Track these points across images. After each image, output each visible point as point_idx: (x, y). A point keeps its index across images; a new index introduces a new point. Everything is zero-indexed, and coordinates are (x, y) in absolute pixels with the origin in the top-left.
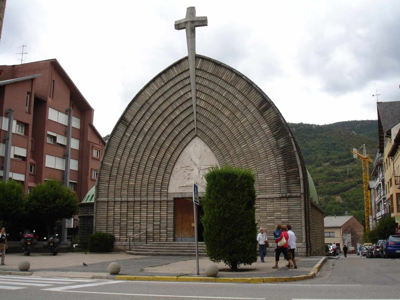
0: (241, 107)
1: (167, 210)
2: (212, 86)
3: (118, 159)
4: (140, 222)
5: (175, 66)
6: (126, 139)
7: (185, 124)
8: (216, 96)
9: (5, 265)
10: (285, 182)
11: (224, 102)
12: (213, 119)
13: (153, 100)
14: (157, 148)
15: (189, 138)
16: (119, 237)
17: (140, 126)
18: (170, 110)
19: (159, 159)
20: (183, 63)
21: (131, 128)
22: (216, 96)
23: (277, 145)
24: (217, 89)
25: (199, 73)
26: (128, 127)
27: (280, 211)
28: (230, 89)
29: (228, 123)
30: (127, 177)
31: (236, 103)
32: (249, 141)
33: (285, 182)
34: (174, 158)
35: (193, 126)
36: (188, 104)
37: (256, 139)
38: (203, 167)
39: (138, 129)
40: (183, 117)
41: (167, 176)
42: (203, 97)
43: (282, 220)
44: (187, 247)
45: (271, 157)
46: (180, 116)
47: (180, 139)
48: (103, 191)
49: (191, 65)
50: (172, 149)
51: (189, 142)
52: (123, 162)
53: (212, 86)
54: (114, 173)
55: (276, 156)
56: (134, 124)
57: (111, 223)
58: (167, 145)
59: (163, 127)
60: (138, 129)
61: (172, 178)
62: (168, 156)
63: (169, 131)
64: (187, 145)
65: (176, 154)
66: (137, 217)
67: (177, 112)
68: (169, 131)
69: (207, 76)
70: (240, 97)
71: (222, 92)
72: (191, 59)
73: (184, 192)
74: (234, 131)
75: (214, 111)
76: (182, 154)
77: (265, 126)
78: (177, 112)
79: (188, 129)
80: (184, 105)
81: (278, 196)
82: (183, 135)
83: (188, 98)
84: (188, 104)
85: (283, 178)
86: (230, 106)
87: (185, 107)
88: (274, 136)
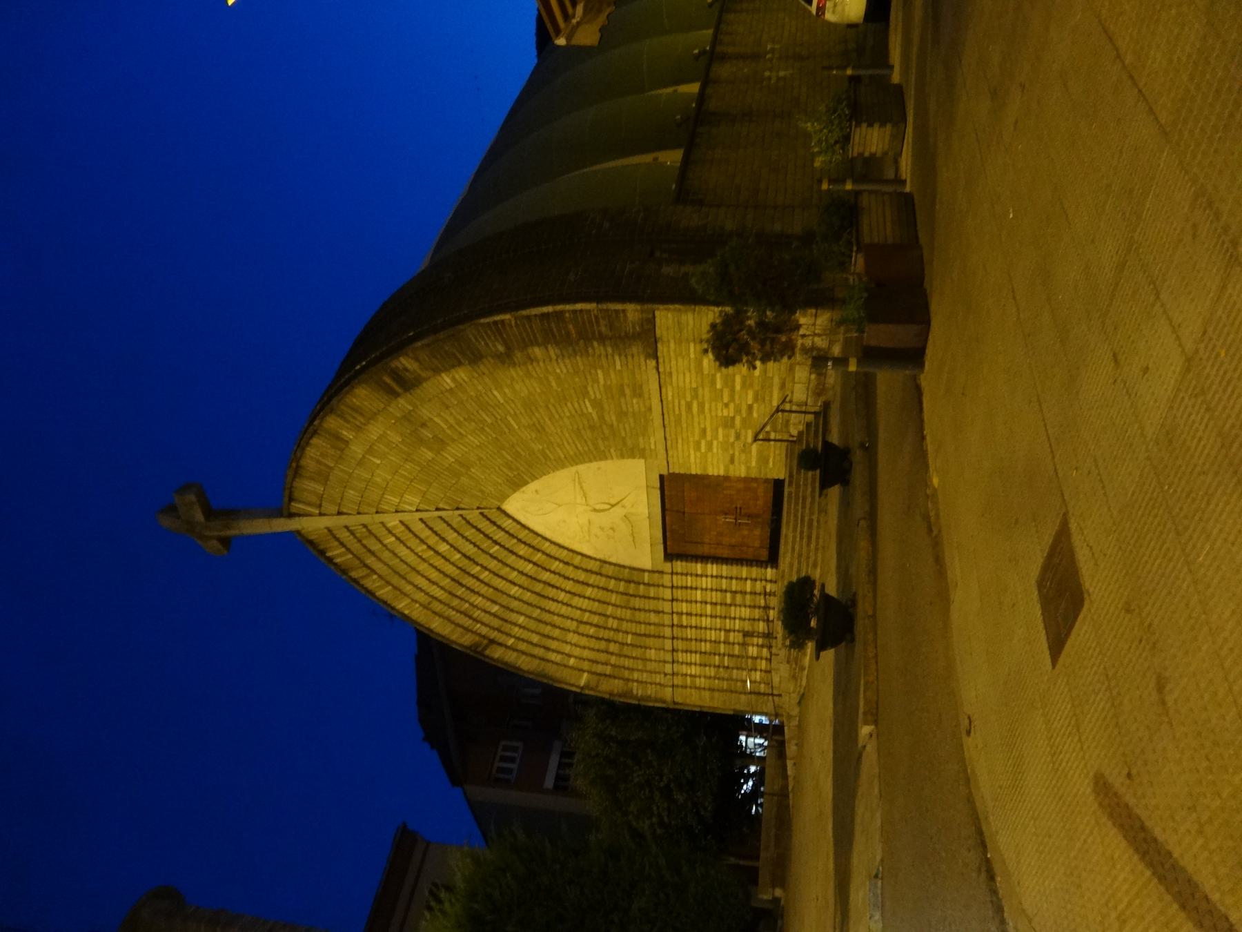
1: (697, 575)
3: (572, 661)
4: (725, 630)
5: (325, 553)
6: (523, 646)
7: (470, 533)
9: (818, 657)
14: (539, 587)
15: (507, 524)
16: (758, 673)
19: (569, 585)
21: (494, 635)
30: (613, 647)
34: (563, 554)
39: (496, 623)
40: (451, 536)
41: (609, 570)
44: (797, 504)
46: (451, 542)
47: (511, 543)
50: (538, 557)
51: (518, 522)
52: (577, 652)
54: (608, 670)
56: (484, 630)
57: (725, 685)
58: (529, 568)
59: (485, 575)
60: (496, 623)
61: (613, 560)
62: (556, 565)
63: (493, 564)
64: (524, 526)
65: (553, 550)
66: (712, 635)
67: (443, 548)
68: (493, 564)
76: (550, 538)
78: (443, 548)
79: (484, 525)
80: (423, 536)
83: (403, 528)
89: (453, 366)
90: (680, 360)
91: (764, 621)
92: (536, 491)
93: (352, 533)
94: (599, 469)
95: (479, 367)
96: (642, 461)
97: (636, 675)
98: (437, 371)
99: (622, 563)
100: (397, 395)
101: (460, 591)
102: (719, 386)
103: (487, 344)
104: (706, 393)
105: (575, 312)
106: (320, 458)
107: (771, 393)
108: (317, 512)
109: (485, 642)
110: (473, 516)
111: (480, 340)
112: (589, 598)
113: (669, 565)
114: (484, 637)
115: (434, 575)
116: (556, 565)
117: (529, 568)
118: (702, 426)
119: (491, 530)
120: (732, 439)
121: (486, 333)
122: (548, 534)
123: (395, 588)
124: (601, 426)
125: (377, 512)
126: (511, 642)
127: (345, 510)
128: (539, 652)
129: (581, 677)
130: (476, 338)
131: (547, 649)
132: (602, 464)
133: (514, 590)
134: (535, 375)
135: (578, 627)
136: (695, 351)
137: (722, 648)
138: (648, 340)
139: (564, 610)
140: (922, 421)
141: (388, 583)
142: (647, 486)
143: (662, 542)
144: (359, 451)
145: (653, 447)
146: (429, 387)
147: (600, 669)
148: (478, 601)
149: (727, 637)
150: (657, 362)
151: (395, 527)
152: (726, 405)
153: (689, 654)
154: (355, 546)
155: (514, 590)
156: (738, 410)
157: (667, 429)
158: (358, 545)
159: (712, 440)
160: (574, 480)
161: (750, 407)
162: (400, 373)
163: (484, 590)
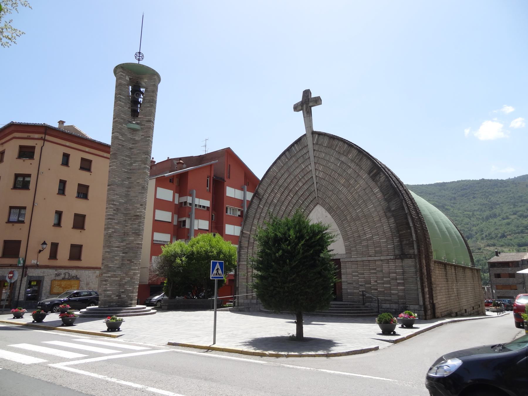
6: (259, 211)
7: (307, 193)
13: (279, 175)
17: (271, 198)
21: (264, 201)
26: (261, 200)
27: (395, 273)
40: (306, 187)
45: (384, 220)
49: (309, 141)
55: (388, 218)
56: (265, 197)
67: (300, 184)
72: (309, 136)
78: (300, 184)
79: (311, 198)
82: (306, 203)
85: (396, 240)
89: (383, 193)
90: (394, 267)
91: (252, 298)
92: (327, 216)
93: (306, 154)
95: (383, 201)
97: (250, 251)
98: (381, 188)
100: (369, 174)
101: (282, 189)
102: (384, 279)
103: (394, 204)
104: (380, 275)
105: (411, 232)
106: (338, 146)
107: (383, 297)
108: (315, 143)
109: (261, 197)
110: (315, 195)
111: (395, 202)
114: (263, 197)
115: (289, 180)
118: (365, 274)
119: (309, 200)
120: (360, 283)
121: (398, 204)
123: (282, 167)
124: (360, 239)
125: (315, 163)
127: (315, 152)
128: (258, 216)
129: (248, 231)
130: (395, 201)
131: (259, 219)
133: (283, 208)
134: (134, 182)
136: (399, 272)
138: (402, 256)
140: (390, 342)
141: (284, 165)
144: (343, 159)
145: (352, 257)
146: (372, 184)
148: (278, 195)
150: (392, 259)
151: (309, 168)
152: (376, 281)
154: (300, 154)
155: (283, 208)
156: (374, 285)
157: (362, 262)
158: (301, 155)
159: (358, 277)
161: (377, 290)
162: (378, 175)
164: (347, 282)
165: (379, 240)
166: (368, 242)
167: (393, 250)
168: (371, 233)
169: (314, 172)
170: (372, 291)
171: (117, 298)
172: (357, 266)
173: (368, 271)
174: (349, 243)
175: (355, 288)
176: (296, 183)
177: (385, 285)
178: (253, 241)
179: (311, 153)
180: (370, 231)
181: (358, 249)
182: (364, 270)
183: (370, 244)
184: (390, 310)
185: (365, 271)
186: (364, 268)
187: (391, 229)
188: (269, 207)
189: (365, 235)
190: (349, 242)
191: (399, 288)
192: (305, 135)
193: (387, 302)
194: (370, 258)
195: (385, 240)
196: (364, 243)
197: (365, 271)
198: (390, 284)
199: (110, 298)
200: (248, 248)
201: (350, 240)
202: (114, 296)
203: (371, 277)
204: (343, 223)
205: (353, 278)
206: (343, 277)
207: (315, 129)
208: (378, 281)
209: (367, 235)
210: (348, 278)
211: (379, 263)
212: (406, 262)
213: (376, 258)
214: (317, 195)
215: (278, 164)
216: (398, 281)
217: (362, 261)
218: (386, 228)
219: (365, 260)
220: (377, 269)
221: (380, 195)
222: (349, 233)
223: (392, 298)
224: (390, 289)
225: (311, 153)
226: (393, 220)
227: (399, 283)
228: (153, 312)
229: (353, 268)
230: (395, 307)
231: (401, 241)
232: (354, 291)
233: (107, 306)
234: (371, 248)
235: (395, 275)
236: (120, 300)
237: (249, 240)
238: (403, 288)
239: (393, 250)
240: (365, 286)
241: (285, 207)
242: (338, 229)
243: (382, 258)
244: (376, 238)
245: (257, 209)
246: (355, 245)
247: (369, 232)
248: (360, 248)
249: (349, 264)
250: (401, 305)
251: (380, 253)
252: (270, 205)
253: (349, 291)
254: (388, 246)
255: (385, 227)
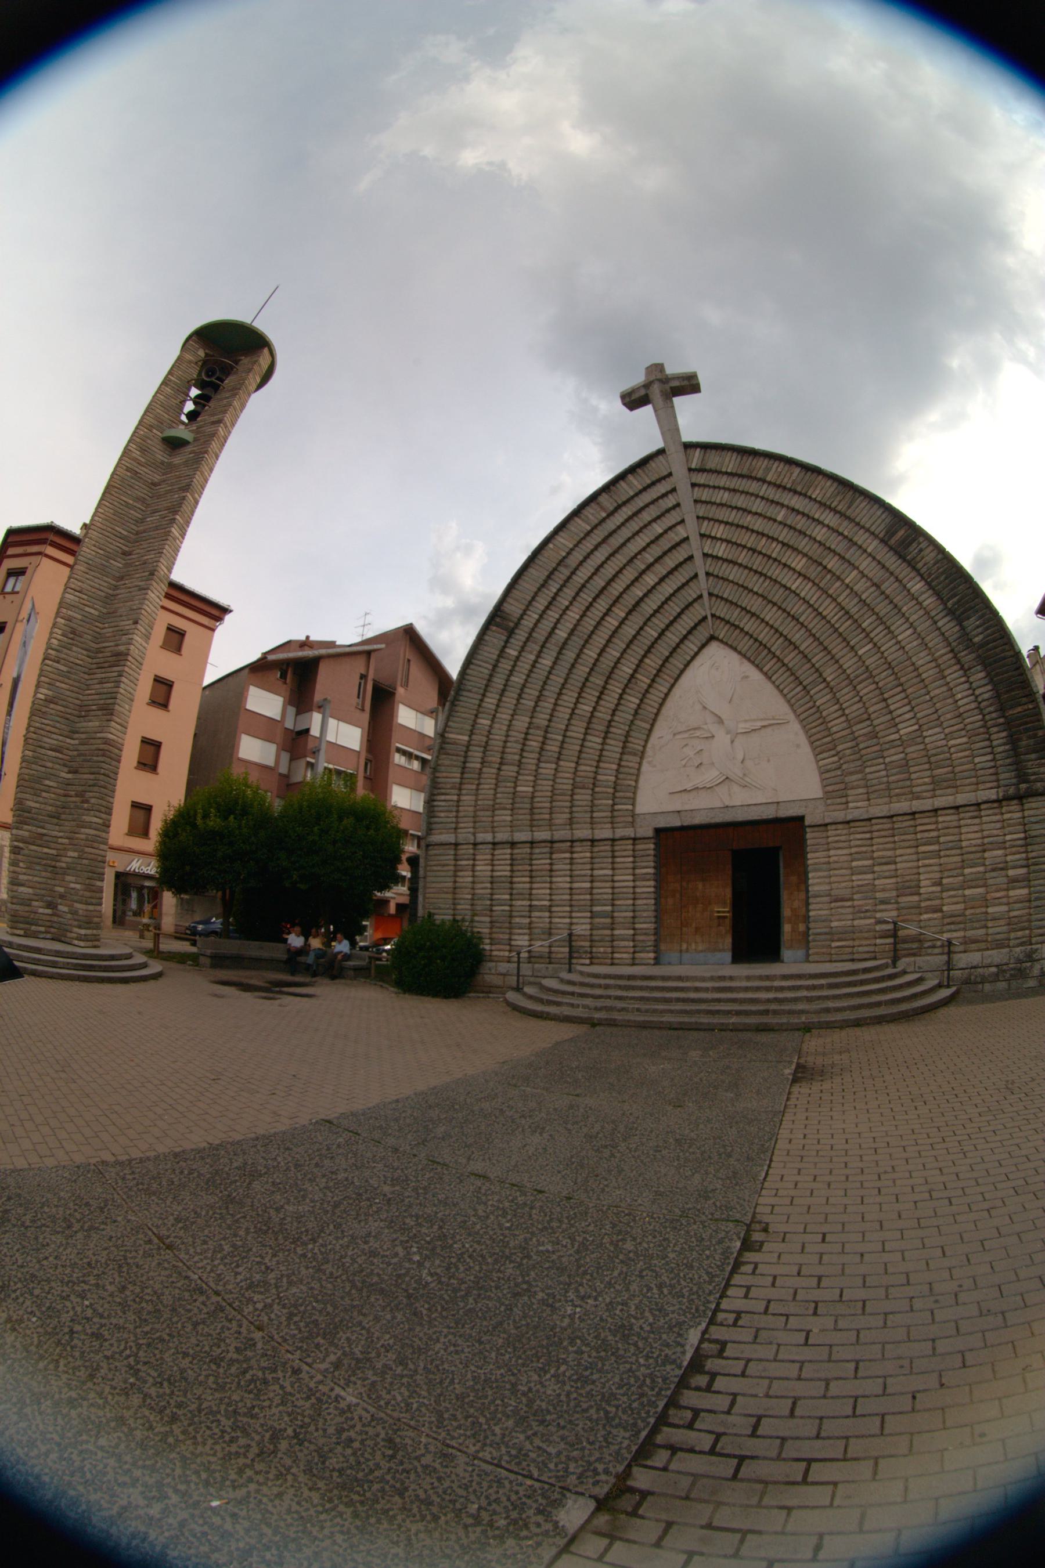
0: (834, 542)
2: (740, 501)
3: (484, 722)
6: (505, 665)
8: (758, 524)
10: (1007, 747)
11: (784, 535)
12: (757, 584)
15: (691, 646)
18: (629, 575)
20: (652, 464)
21: (521, 635)
22: (758, 524)
23: (965, 637)
24: (758, 506)
25: (701, 479)
26: (511, 633)
27: (1002, 845)
28: (796, 502)
29: (806, 590)
30: (509, 770)
31: (820, 533)
32: (878, 634)
33: (1007, 747)
34: (650, 709)
35: (698, 611)
36: (680, 555)
37: (897, 625)
38: (742, 725)
42: (719, 531)
43: (1011, 873)
45: (954, 675)
48: (442, 815)
49: (677, 463)
50: (643, 680)
51: (693, 658)
52: (500, 730)
53: (740, 501)
54: (474, 764)
55: (965, 670)
56: (528, 623)
59: (612, 622)
60: (540, 635)
62: (632, 701)
63: (629, 631)
65: (655, 696)
68: (629, 631)
69: (723, 481)
70: (829, 518)
71: (771, 511)
73: (687, 807)
74: (828, 608)
75: (757, 563)
77: (917, 586)
78: (650, 579)
81: (992, 795)
84: (680, 555)
85: (999, 737)
86: (803, 544)
87: (670, 562)
88: (951, 612)
94: (798, 746)
96: (820, 794)
97: (467, 799)
99: (33, 978)
112: (783, 505)
113: (650, 833)
116: (632, 701)
117: (627, 669)
120: (878, 895)
122: (677, 691)
126: (513, 652)
132: (806, 749)
135: (538, 728)
137: (521, 904)
139: (564, 713)
142: (778, 803)
143: (685, 824)
147: (476, 754)
149: (541, 909)
153: (548, 717)
160: (774, 719)
163: (589, 623)
164: (829, 895)
165: (944, 742)
166: (908, 750)
167: (991, 771)
168: (914, 721)
169: (695, 540)
170: (925, 916)
171: (49, 911)
172: (868, 836)
173: (909, 851)
174: (835, 759)
175: (859, 912)
176: (749, 545)
177: (967, 892)
178: (478, 766)
179: (685, 495)
180: (911, 715)
181: (869, 776)
182: (895, 849)
183: (914, 755)
184: (979, 970)
185: (898, 852)
186: (896, 838)
187: (980, 703)
188: (540, 652)
189: (893, 730)
190: (834, 756)
191: (1011, 893)
192: (661, 452)
193: (974, 946)
194: (917, 805)
195: (965, 740)
196: (894, 756)
197: (898, 852)
198: (985, 886)
199: (27, 908)
200: (460, 789)
201: (839, 748)
202: (41, 904)
203: (921, 870)
204: (812, 692)
205: (854, 878)
206: (813, 878)
207: (686, 437)
208: (945, 881)
209: (900, 726)
210: (833, 879)
211: (948, 818)
212: (1034, 805)
213: (939, 802)
214: (711, 609)
215: (571, 527)
216: (1011, 873)
217: (888, 817)
218: (965, 702)
219: (901, 812)
220: (942, 839)
221: (929, 600)
222: (837, 725)
223: (991, 931)
224: (986, 902)
225: (685, 495)
226: (982, 674)
227: (1014, 880)
228: (140, 964)
229: (853, 843)
230: (997, 960)
231: (1013, 741)
232: (856, 923)
233: (22, 932)
234: (916, 768)
235: (1000, 852)
236: (55, 919)
237: (464, 763)
238: (1025, 891)
239: (991, 771)
240: (897, 903)
241: (598, 651)
242: (791, 716)
243: (961, 799)
244: (933, 736)
245: (498, 661)
246: (859, 763)
247: (907, 716)
248: (877, 774)
249: (839, 832)
250: (1018, 949)
251: (952, 783)
252: (543, 647)
253: (834, 924)
254: (977, 760)
255: (959, 696)
